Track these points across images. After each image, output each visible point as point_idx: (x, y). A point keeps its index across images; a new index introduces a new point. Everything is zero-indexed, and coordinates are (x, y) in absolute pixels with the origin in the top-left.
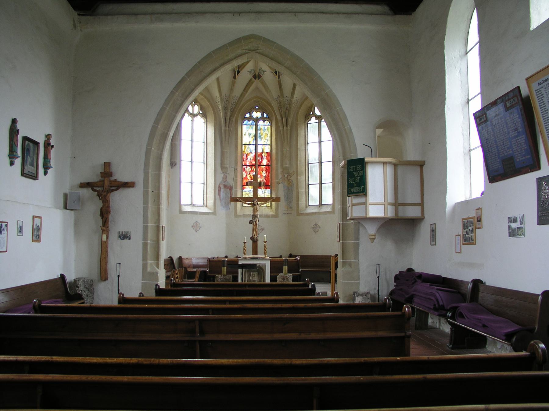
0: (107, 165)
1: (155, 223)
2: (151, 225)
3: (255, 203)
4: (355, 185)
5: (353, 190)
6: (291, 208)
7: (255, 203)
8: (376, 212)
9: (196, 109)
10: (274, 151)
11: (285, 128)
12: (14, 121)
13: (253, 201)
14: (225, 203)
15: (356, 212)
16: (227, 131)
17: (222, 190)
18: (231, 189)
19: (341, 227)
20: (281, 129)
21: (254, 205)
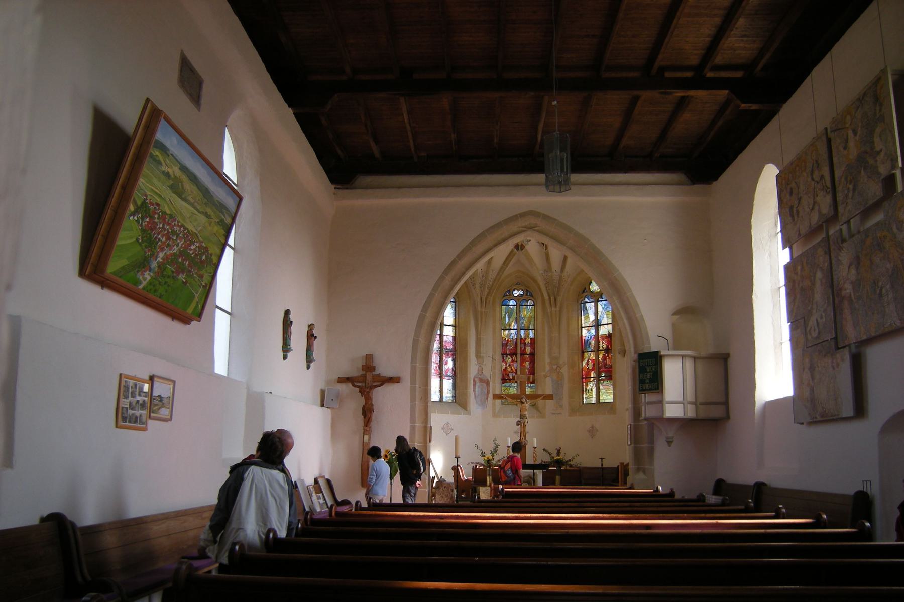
0: (369, 357)
4: (647, 381)
5: (646, 386)
6: (561, 406)
7: (524, 400)
8: (673, 411)
12: (287, 313)
15: (649, 412)
17: (478, 384)
18: (488, 383)
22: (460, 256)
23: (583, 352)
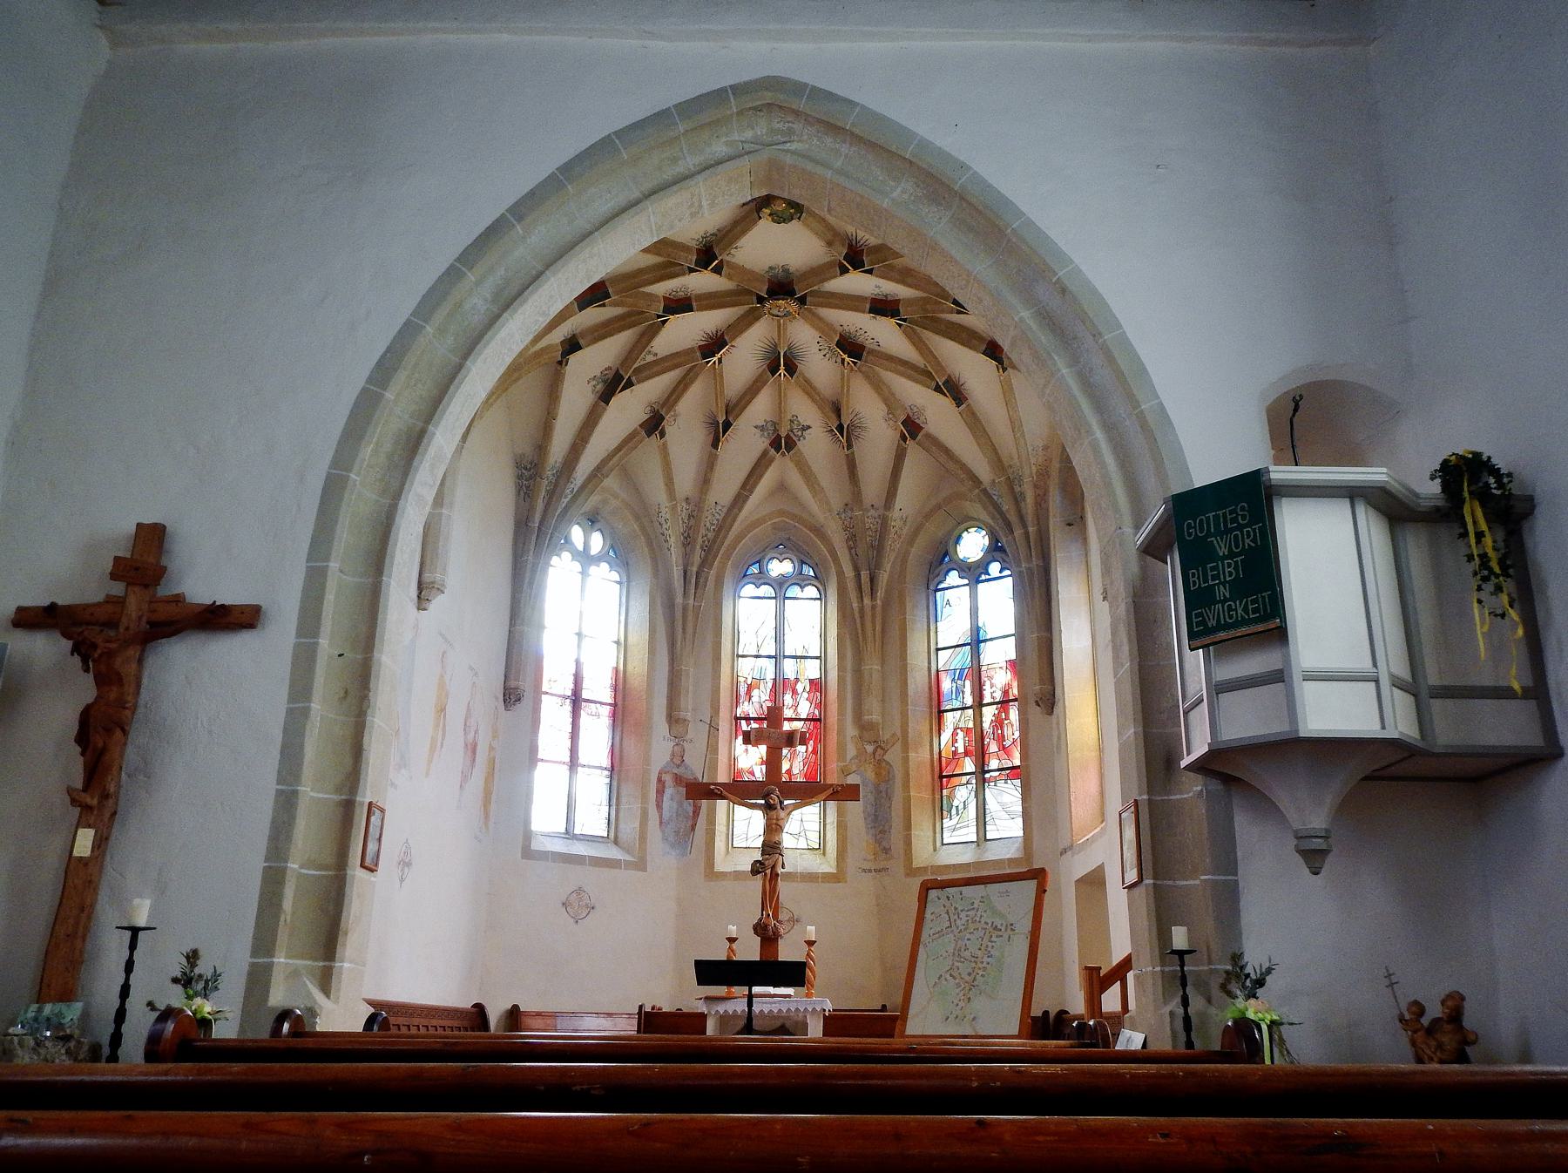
0: (152, 537)
1: (338, 790)
2: (314, 794)
3: (774, 799)
4: (1223, 592)
6: (886, 850)
7: (774, 799)
8: (1336, 711)
9: (597, 542)
10: (833, 675)
11: (867, 601)
13: (766, 796)
14: (677, 833)
16: (690, 613)
19: (1144, 816)
20: (855, 605)
21: (768, 808)
22: (524, 208)
23: (941, 712)
